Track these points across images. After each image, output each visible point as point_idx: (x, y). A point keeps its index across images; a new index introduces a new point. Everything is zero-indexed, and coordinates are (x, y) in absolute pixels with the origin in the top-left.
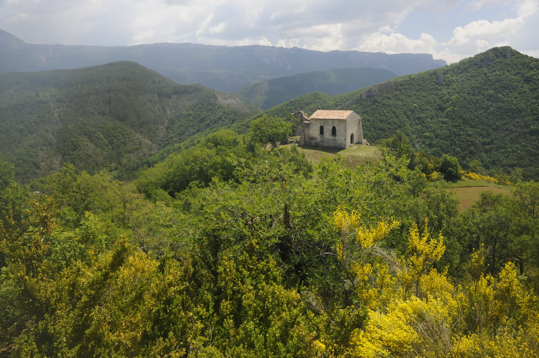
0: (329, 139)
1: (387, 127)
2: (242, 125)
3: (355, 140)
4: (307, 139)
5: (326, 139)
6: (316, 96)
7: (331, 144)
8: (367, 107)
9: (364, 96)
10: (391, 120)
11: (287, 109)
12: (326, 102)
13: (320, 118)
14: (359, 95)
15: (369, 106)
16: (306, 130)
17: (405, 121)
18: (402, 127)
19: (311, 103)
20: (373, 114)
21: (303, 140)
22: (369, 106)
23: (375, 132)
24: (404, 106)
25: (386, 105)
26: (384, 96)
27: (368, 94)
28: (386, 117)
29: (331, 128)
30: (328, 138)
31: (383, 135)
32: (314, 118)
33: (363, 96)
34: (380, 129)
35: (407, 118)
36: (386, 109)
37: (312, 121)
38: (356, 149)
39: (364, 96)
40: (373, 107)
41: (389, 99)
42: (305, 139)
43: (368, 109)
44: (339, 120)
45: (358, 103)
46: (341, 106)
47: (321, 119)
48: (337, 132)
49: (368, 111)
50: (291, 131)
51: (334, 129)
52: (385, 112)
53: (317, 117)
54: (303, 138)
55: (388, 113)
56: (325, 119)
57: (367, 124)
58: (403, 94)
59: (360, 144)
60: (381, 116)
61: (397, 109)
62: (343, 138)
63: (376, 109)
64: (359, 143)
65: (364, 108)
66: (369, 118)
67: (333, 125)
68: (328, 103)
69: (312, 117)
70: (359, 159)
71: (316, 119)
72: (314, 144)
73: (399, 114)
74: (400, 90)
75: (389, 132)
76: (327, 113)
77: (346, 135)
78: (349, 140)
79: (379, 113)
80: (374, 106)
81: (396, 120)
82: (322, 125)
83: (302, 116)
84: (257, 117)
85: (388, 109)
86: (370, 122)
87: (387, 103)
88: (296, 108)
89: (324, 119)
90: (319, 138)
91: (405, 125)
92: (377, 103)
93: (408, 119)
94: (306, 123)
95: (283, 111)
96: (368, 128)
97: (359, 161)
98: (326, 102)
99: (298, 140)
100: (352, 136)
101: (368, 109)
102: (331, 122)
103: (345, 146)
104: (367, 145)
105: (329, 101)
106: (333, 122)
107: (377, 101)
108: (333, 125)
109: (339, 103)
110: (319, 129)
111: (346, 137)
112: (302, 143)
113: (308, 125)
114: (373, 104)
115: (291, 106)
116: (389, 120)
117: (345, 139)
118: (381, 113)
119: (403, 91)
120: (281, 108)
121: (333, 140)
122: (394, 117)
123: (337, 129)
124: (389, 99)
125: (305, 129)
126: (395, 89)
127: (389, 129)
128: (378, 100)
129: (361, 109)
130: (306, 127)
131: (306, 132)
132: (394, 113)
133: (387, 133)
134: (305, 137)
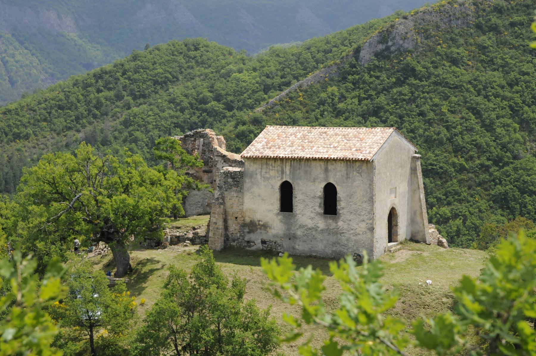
0: (315, 229)
1: (454, 165)
3: (402, 231)
4: (233, 227)
5: (302, 226)
6: (192, 53)
8: (378, 94)
9: (366, 55)
10: (467, 138)
11: (88, 103)
12: (228, 75)
13: (282, 154)
14: (349, 50)
15: (386, 90)
16: (231, 197)
17: (517, 141)
18: (507, 164)
19: (175, 80)
21: (221, 231)
22: (386, 90)
24: (511, 85)
25: (447, 85)
26: (438, 54)
27: (381, 47)
28: (448, 128)
29: (319, 189)
30: (310, 223)
32: (257, 154)
33: (362, 53)
35: (522, 129)
36: (446, 98)
37: (251, 167)
38: (408, 262)
39: (366, 55)
40: (401, 94)
41: (455, 62)
42: (226, 228)
43: (382, 99)
45: (344, 79)
46: (287, 91)
47: (282, 160)
48: (341, 205)
49: (382, 108)
50: (175, 201)
52: (445, 109)
54: (220, 224)
55: (452, 112)
56: (300, 160)
58: (505, 43)
59: (417, 242)
60: (430, 123)
61: (486, 97)
62: (363, 225)
63: (410, 101)
65: (370, 97)
68: (238, 80)
69: (251, 151)
70: (427, 299)
71: (268, 159)
72: (259, 245)
73: (493, 116)
74: (494, 29)
75: (460, 182)
76: (304, 137)
77: (372, 212)
78: (382, 230)
79: (422, 114)
80: (405, 89)
81: (485, 139)
82: (287, 178)
83: (208, 146)
85: (453, 99)
87: (452, 80)
88: (119, 97)
89: (293, 159)
91: (516, 157)
92: (416, 77)
93: (525, 134)
94: (228, 174)
95: (71, 106)
97: (425, 306)
98: (228, 75)
99: (201, 232)
100: (392, 216)
101: (382, 99)
104: (440, 244)
105: (240, 71)
106: (326, 170)
107: (413, 70)
108: (327, 177)
109: (277, 80)
110: (277, 195)
111: (373, 219)
114: (399, 83)
115: (99, 91)
116: (459, 139)
117: (372, 229)
118: (431, 115)
119: (507, 35)
120: (62, 96)
121: (327, 231)
122: (478, 127)
123: (341, 193)
124: (455, 62)
126: (479, 27)
127: (461, 169)
128: (419, 68)
129: (356, 101)
130: (230, 187)
131: (228, 203)
132: (477, 113)
133: (453, 185)
134: (225, 221)
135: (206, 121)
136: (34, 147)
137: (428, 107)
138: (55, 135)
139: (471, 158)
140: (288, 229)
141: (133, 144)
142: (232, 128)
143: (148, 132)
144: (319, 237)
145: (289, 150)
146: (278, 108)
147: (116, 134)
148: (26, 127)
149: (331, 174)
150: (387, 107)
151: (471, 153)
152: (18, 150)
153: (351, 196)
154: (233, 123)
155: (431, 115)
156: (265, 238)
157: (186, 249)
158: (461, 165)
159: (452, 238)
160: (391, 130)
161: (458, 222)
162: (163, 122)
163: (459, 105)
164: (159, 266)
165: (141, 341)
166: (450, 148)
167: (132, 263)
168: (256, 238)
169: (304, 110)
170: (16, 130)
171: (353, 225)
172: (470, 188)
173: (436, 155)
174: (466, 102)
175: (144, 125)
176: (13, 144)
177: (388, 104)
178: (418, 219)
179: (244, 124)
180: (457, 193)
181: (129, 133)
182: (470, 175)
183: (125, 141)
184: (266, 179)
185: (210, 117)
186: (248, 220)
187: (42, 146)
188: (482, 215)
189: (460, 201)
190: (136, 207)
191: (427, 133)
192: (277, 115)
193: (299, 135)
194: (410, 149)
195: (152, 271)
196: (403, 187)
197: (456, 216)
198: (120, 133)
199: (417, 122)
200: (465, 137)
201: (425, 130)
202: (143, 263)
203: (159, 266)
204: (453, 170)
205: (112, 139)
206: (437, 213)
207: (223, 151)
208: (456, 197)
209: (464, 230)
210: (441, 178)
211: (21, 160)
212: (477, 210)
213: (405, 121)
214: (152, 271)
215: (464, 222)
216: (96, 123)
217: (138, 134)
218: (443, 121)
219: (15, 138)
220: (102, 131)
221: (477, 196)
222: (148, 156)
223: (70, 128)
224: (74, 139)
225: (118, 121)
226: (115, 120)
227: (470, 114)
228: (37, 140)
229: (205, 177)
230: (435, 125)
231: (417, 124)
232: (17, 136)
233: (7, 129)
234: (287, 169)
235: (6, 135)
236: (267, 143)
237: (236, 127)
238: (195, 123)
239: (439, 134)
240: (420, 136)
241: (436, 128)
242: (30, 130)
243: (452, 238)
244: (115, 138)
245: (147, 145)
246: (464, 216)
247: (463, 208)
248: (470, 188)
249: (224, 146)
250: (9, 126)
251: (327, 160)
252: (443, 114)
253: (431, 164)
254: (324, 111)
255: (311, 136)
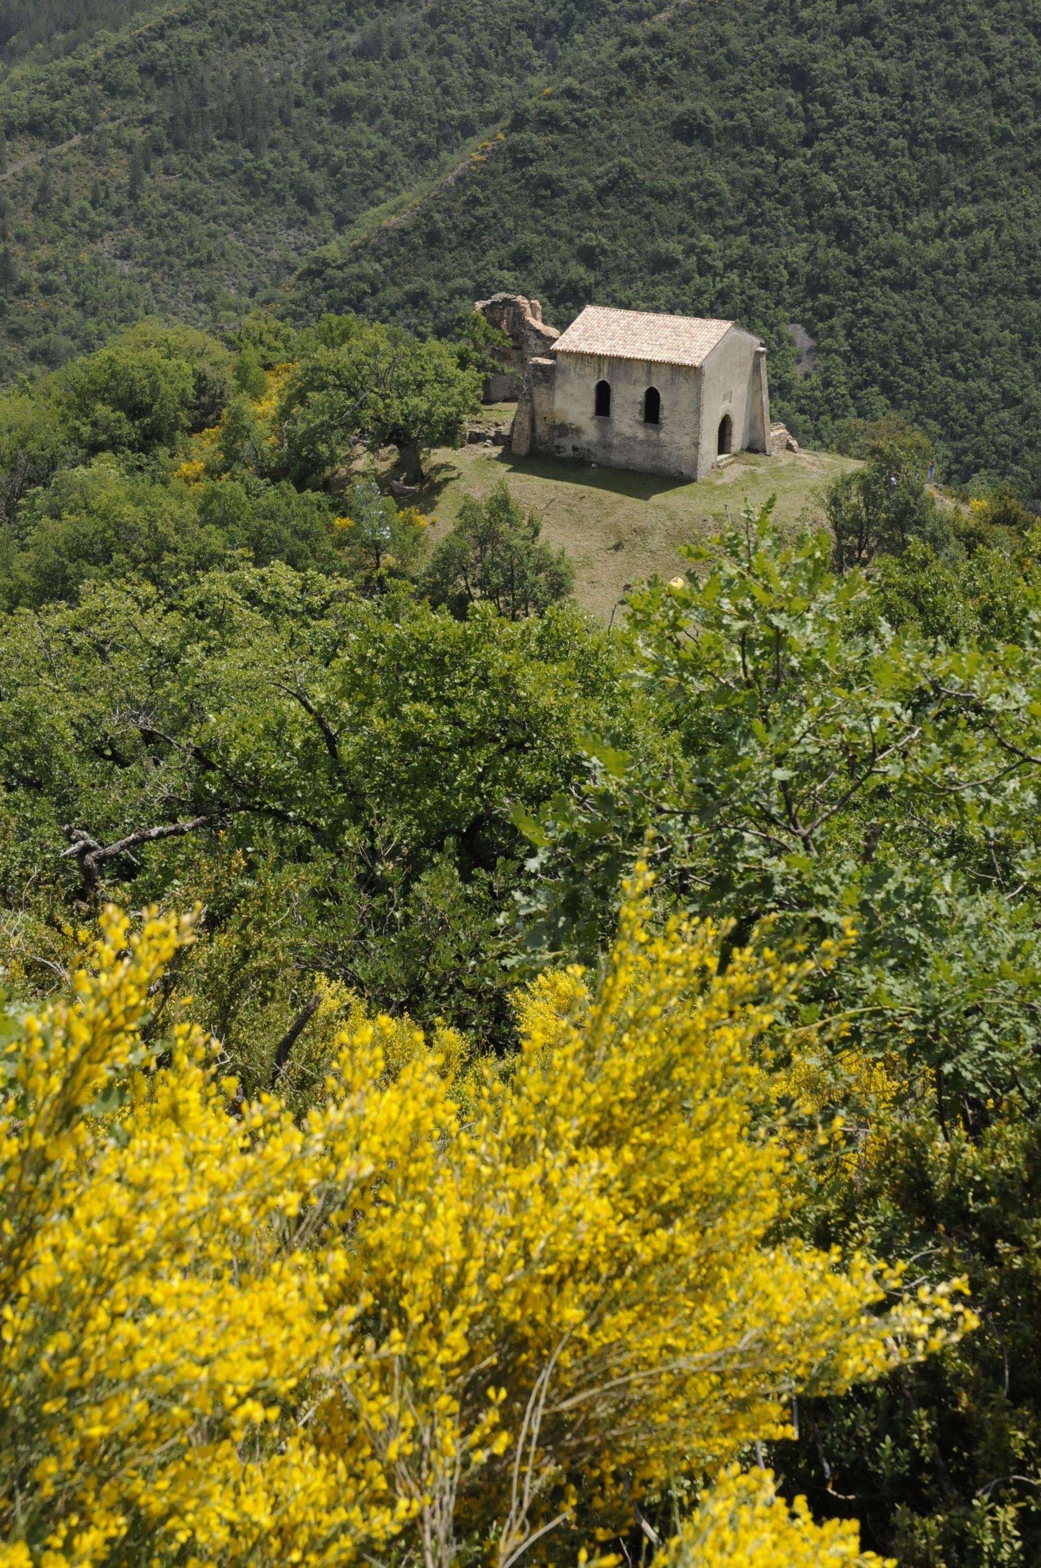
0: (634, 438)
1: (991, 130)
2: (74, 73)
3: (738, 438)
4: (541, 429)
5: (619, 434)
7: (639, 458)
13: (599, 349)
16: (540, 395)
20: (908, 38)
23: (914, 157)
28: (988, 61)
30: (628, 432)
31: (961, 183)
34: (944, 144)
38: (737, 483)
42: (533, 428)
44: (676, 368)
47: (601, 357)
48: (664, 414)
51: (652, 400)
53: (585, 347)
54: (526, 424)
56: (620, 359)
57: (866, 108)
59: (756, 452)
60: (957, 51)
64: (755, 448)
66: (880, 65)
67: (649, 381)
75: (998, 161)
77: (697, 425)
82: (604, 377)
83: (518, 316)
84: (171, 22)
86: (883, 92)
90: (591, 432)
94: (537, 367)
96: (871, 131)
99: (505, 430)
100: (725, 426)
102: (640, 373)
103: (695, 466)
104: (789, 447)
108: (649, 381)
110: (592, 396)
111: (698, 433)
112: (522, 448)
113: (547, 376)
116: (1004, 83)
117: (697, 444)
118: (962, 36)
121: (647, 442)
123: (664, 400)
125: (535, 390)
127: (1003, 139)
130: (538, 383)
131: (537, 400)
134: (533, 421)
135: (574, 18)
136: (276, 58)
137: (957, 20)
138: (310, 35)
139: (1023, 118)
140: (604, 436)
141: (445, 59)
142: (613, 51)
143: (472, 35)
144: (638, 448)
145: (608, 343)
146: (696, 14)
147: (416, 37)
148: (262, 19)
149: (654, 379)
150: (886, 20)
151: (1024, 109)
152: (250, 63)
153: (675, 404)
154: (616, 40)
155: (962, 36)
156: (577, 444)
157: (487, 451)
158: (1004, 130)
159: (974, 262)
160: (727, 325)
161: (988, 233)
162: (498, 18)
163: (1012, 17)
164: (454, 474)
165: (430, 575)
166: (988, 99)
167: (425, 469)
168: (567, 443)
169: (741, 20)
170: (244, 25)
171: (677, 438)
172: (1014, 173)
173: (963, 112)
174: (1025, 12)
175: (465, 23)
176: (240, 50)
177: (888, 13)
178: (759, 424)
179: (635, 43)
180: (990, 182)
181: (439, 36)
182: (1017, 149)
183: (430, 51)
184: (581, 377)
185: (581, 11)
186: (558, 422)
187: (288, 56)
188: (1030, 222)
189: (995, 197)
190: (429, 413)
191: (950, 70)
192: (693, 29)
193: (623, 323)
194: (753, 342)
195: (447, 480)
196: (741, 389)
197: (984, 223)
198: (423, 36)
199: (935, 50)
200: (1017, 79)
201: (949, 64)
202: (438, 469)
203: (454, 474)
204: (988, 139)
205: (408, 48)
206: (953, 217)
207: (538, 325)
208: (989, 189)
209: (995, 248)
210: (967, 154)
211: (253, 81)
212: (1021, 214)
213: (914, 47)
214: (447, 480)
215: (998, 235)
216: (381, 17)
217: (452, 39)
218: (982, 48)
219: (244, 40)
220: (391, 32)
221: (1025, 188)
222: (470, 80)
223: (336, 25)
224: (343, 44)
225: (419, 14)
226: (414, 11)
227: (1031, 36)
228: (281, 44)
229: (514, 355)
230: (966, 55)
231: (934, 52)
232: (247, 38)
233: (230, 23)
234: (605, 368)
235: (229, 33)
236: (585, 331)
237: (620, 49)
238: (553, 22)
239: (971, 72)
240: (938, 75)
241: (970, 60)
242: (268, 26)
243: (974, 262)
244: (415, 45)
245: (468, 61)
246: (1000, 224)
247: (998, 209)
248: (1014, 173)
249: (539, 315)
250: (233, 17)
251: (650, 363)
252: (983, 35)
253: (952, 128)
254: (776, 22)
255: (636, 325)
